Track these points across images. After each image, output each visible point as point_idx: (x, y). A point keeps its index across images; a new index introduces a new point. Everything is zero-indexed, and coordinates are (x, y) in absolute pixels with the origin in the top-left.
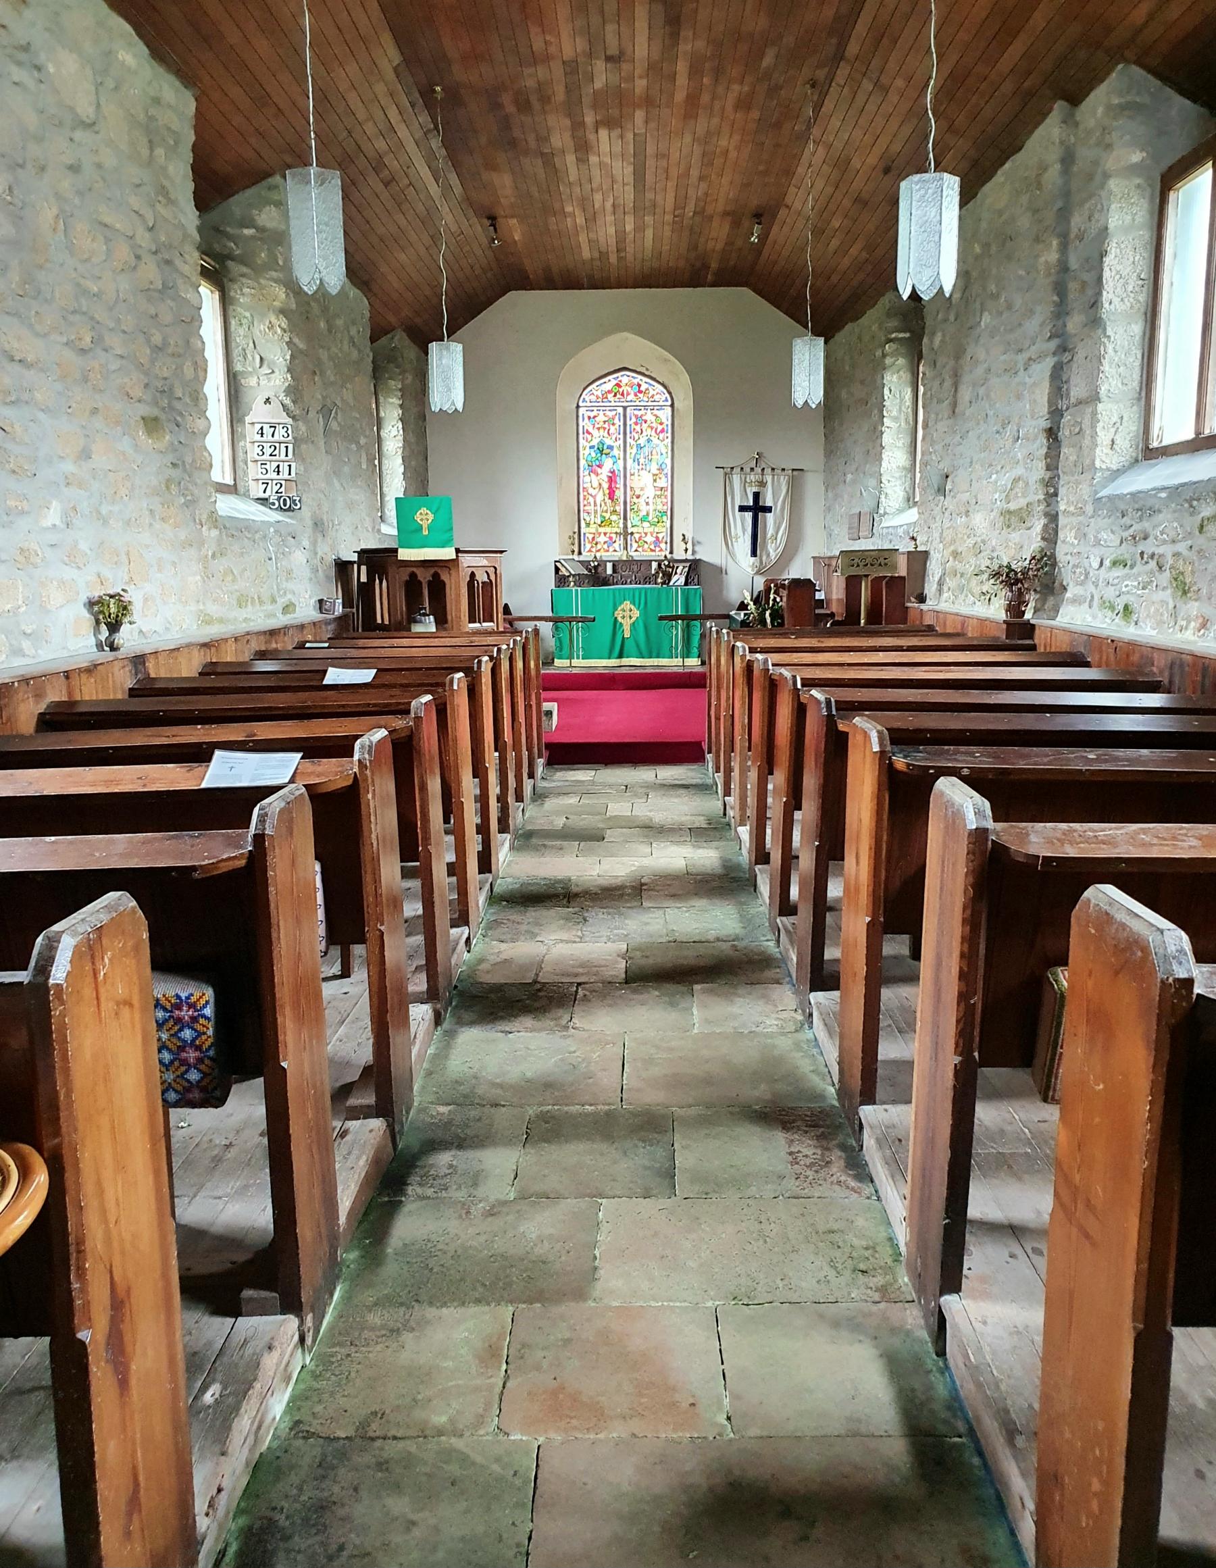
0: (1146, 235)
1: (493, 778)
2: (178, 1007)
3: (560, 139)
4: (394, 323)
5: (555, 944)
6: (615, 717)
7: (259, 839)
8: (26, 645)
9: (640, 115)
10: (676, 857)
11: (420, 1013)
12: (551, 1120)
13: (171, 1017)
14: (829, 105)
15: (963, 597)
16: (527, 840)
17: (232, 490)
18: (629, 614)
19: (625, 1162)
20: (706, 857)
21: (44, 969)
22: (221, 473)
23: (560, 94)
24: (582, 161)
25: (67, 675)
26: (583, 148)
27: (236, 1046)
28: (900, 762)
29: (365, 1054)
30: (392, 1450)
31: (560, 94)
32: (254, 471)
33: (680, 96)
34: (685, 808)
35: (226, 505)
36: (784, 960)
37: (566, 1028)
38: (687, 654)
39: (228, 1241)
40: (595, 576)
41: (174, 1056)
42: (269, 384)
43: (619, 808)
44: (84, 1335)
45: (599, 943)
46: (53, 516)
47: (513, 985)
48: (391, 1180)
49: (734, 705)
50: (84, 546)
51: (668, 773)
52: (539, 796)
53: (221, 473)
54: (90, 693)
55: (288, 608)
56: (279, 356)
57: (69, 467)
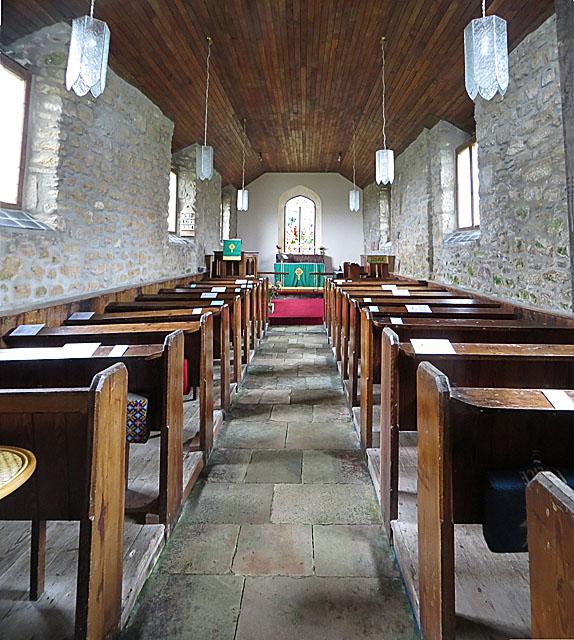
0: (453, 166)
1: (249, 330)
2: (136, 405)
3: (281, 132)
4: (229, 182)
5: (268, 390)
6: (298, 307)
7: (166, 347)
8: (105, 284)
9: (304, 127)
10: (310, 358)
11: (218, 414)
12: (263, 453)
13: (132, 409)
14: (359, 125)
15: (411, 267)
16: (259, 353)
17: (174, 233)
18: (299, 272)
19: (280, 469)
20: (321, 359)
21: (95, 387)
22: (172, 228)
23: (280, 122)
24: (287, 138)
25: (116, 294)
26: (287, 136)
27: (152, 422)
28: (376, 323)
29: (198, 428)
30: (192, 579)
31: (280, 122)
32: (182, 228)
33: (316, 122)
34: (315, 341)
35: (172, 239)
36: (345, 395)
37: (268, 420)
38: (319, 286)
39: (144, 496)
40: (292, 259)
41: (132, 422)
42: (189, 202)
43: (293, 341)
44: (92, 518)
45: (282, 389)
46: (118, 244)
47: (67, 65)
48: (202, 476)
49: (331, 303)
50: (126, 253)
51: (310, 328)
52: (265, 337)
53: (172, 228)
54: (123, 300)
55: (189, 271)
56: (192, 194)
57: (125, 229)
